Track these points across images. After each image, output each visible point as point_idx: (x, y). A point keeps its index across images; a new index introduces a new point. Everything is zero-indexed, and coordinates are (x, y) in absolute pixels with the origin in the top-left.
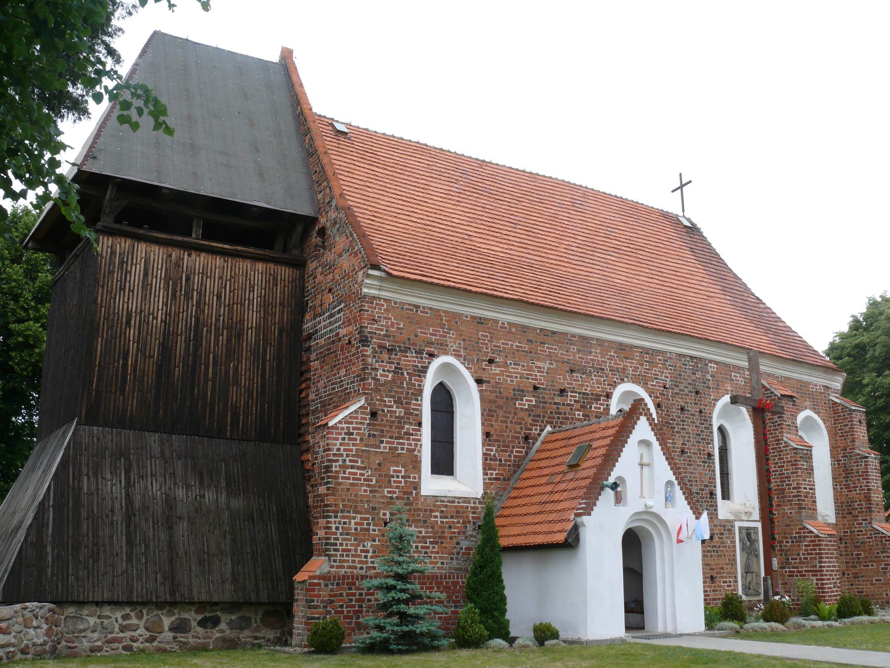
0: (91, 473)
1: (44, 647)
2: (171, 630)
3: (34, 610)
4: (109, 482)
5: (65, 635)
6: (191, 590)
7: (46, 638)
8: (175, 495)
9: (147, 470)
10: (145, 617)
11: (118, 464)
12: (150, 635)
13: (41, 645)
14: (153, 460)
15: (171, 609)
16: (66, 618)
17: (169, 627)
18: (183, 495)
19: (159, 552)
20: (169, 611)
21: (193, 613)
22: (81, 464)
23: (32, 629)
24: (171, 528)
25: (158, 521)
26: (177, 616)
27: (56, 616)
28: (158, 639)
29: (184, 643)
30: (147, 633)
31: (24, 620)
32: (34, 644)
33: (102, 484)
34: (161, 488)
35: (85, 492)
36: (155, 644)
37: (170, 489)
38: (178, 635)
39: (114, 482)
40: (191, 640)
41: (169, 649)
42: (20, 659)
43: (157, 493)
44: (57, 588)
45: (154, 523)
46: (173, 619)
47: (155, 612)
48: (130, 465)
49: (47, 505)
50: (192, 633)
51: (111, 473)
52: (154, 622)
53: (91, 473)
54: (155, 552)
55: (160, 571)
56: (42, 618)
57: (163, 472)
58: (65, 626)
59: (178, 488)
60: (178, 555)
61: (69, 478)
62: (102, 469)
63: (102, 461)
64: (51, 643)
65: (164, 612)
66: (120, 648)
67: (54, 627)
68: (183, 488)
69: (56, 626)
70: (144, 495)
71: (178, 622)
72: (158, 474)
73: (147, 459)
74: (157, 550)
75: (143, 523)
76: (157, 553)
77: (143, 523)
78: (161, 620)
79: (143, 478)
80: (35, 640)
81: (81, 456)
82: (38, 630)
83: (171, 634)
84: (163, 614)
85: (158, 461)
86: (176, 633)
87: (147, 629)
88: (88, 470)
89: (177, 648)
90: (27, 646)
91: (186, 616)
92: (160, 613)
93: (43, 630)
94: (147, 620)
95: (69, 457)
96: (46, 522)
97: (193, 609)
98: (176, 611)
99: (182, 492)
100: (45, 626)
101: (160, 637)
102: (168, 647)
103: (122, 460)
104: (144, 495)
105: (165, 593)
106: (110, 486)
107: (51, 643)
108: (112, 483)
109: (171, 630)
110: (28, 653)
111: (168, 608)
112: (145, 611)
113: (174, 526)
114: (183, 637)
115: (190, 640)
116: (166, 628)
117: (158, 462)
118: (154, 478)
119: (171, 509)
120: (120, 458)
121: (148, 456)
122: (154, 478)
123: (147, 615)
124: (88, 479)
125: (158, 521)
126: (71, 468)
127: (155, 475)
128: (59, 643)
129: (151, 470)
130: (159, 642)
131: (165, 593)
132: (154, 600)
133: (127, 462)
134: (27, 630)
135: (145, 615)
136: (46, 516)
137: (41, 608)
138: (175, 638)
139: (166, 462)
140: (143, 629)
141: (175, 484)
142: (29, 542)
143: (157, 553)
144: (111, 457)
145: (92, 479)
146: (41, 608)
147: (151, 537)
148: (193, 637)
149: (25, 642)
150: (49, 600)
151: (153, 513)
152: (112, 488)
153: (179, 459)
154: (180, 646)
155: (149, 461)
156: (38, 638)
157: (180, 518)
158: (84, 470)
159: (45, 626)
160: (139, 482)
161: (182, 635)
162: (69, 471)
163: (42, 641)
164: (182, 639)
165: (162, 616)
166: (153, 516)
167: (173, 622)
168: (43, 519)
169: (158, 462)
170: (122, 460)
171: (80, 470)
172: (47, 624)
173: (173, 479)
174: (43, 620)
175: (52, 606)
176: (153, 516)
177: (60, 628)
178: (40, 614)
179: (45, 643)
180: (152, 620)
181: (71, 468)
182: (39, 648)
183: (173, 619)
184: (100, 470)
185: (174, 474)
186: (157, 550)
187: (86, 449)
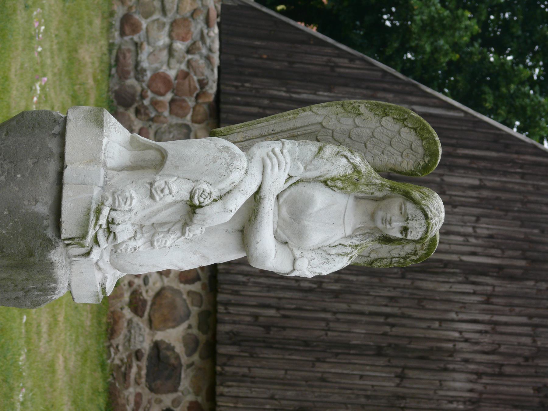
0: (485, 193)
1: (132, 74)
2: (157, 346)
3: (204, 42)
4: (470, 230)
5: (154, 126)
6: (241, 379)
7: (149, 74)
8: (454, 370)
9: (504, 315)
10: (184, 288)
11: (510, 253)
12: (145, 302)
13: (137, 64)
14: (527, 330)
15: (201, 346)
16: (187, 126)
17: (162, 342)
18: (455, 390)
19: (323, 319)
20: (197, 342)
21: (190, 398)
22: (505, 173)
23: (167, 40)
24: (379, 352)
25: (393, 325)
26: (184, 360)
27: (191, 103)
28: (136, 319)
29: (125, 376)
30: (152, 293)
31: (185, 19)
32: (138, 46)
33: (464, 215)
34: (466, 340)
35: (447, 179)
36: (128, 313)
37: (466, 361)
38: (144, 363)
39: (473, 240)
40: (131, 391)
41: (114, 342)
42: (112, 14)
43: (455, 330)
44: (247, 104)
45: (387, 316)
46: (179, 349)
47: (195, 310)
48: (512, 278)
49: (414, 99)
50: (147, 394)
51: (491, 237)
52: (173, 306)
53: (485, 193)
54: (325, 310)
55: (284, 317)
56: (189, 63)
57: (503, 349)
58: (171, 126)
59: (471, 381)
60: (318, 360)
61: (473, 148)
62: (498, 217)
63: (514, 219)
64: (139, 89)
65: (195, 331)
66: (139, 363)
67: (169, 96)
68: (471, 391)
69: (172, 101)
70: (449, 301)
71: (173, 361)
72: (497, 338)
73: (530, 317)
74: (329, 316)
75: (385, 293)
76: (322, 315)
77: (385, 293)
78: (177, 323)
79: (487, 302)
80: (147, 49)
81: (523, 176)
82: (164, 54)
83: (146, 346)
84: (190, 327)
85: (527, 340)
86: (150, 358)
87: (159, 294)
88: (493, 189)
89: (117, 362)
90: (136, 28)
91: (185, 383)
92: (193, 320)
93: (164, 68)
94: (178, 292)
95: (517, 153)
96: (380, 94)
97: (199, 399)
98: (196, 357)
99: (461, 390)
100: (172, 73)
101: (141, 323)
102: (120, 339)
103: (522, 263)
104: (449, 301)
105: (234, 322)
106: (462, 230)
107: (139, 89)
108: (470, 235)
109: (157, 346)
110: (123, 34)
111: (203, 338)
112: (196, 287)
113: (382, 362)
114: (139, 373)
115: (131, 389)
116: (160, 336)
117: (524, 340)
118: (488, 328)
119: (421, 358)
120: (525, 258)
121: (536, 321)
122: (488, 328)
123: (189, 293)
124: (473, 188)
125: (393, 325)
126: (494, 154)
127: (494, 332)
128: (137, 112)
129: (506, 324)
130: (130, 322)
131: (234, 322)
132: (221, 297)
133: (519, 272)
134: (167, 28)
135: (189, 287)
136: (390, 96)
137: (208, 59)
138: (138, 355)
139: (527, 359)
140: (159, 285)
141: (480, 375)
142: (337, 60)
143: (322, 315)
144: (527, 240)
145: (474, 194)
146: (208, 59)
147: (355, 307)
148: (139, 396)
149: (144, 24)
150: (222, 87)
151: (409, 317)
152: (459, 234)
153: (538, 390)
154: (119, 367)
155: (524, 320)
156: (150, 54)
157: (401, 377)
158: (493, 180)
159: (172, 73)
160: (475, 293)
161: (144, 372)
162: (488, 149)
163: (145, 64)
164: (134, 370)
165: (185, 325)
166: (403, 316)
167: (172, 349)
168: (385, 90)
169: (524, 340)
170: (522, 263)
171: (493, 172)
172: (177, 78)
173: (489, 370)
174: (183, 67)
175: (212, 89)
176: (403, 316)
177: (166, 113)
178: (196, 57)
179: (139, 72)
180: (179, 302)
181: (494, 154)
182: (130, 61)
183: (179, 349)
184: (494, 212)
185: (501, 375)
186: (329, 316)
187: (537, 188)
